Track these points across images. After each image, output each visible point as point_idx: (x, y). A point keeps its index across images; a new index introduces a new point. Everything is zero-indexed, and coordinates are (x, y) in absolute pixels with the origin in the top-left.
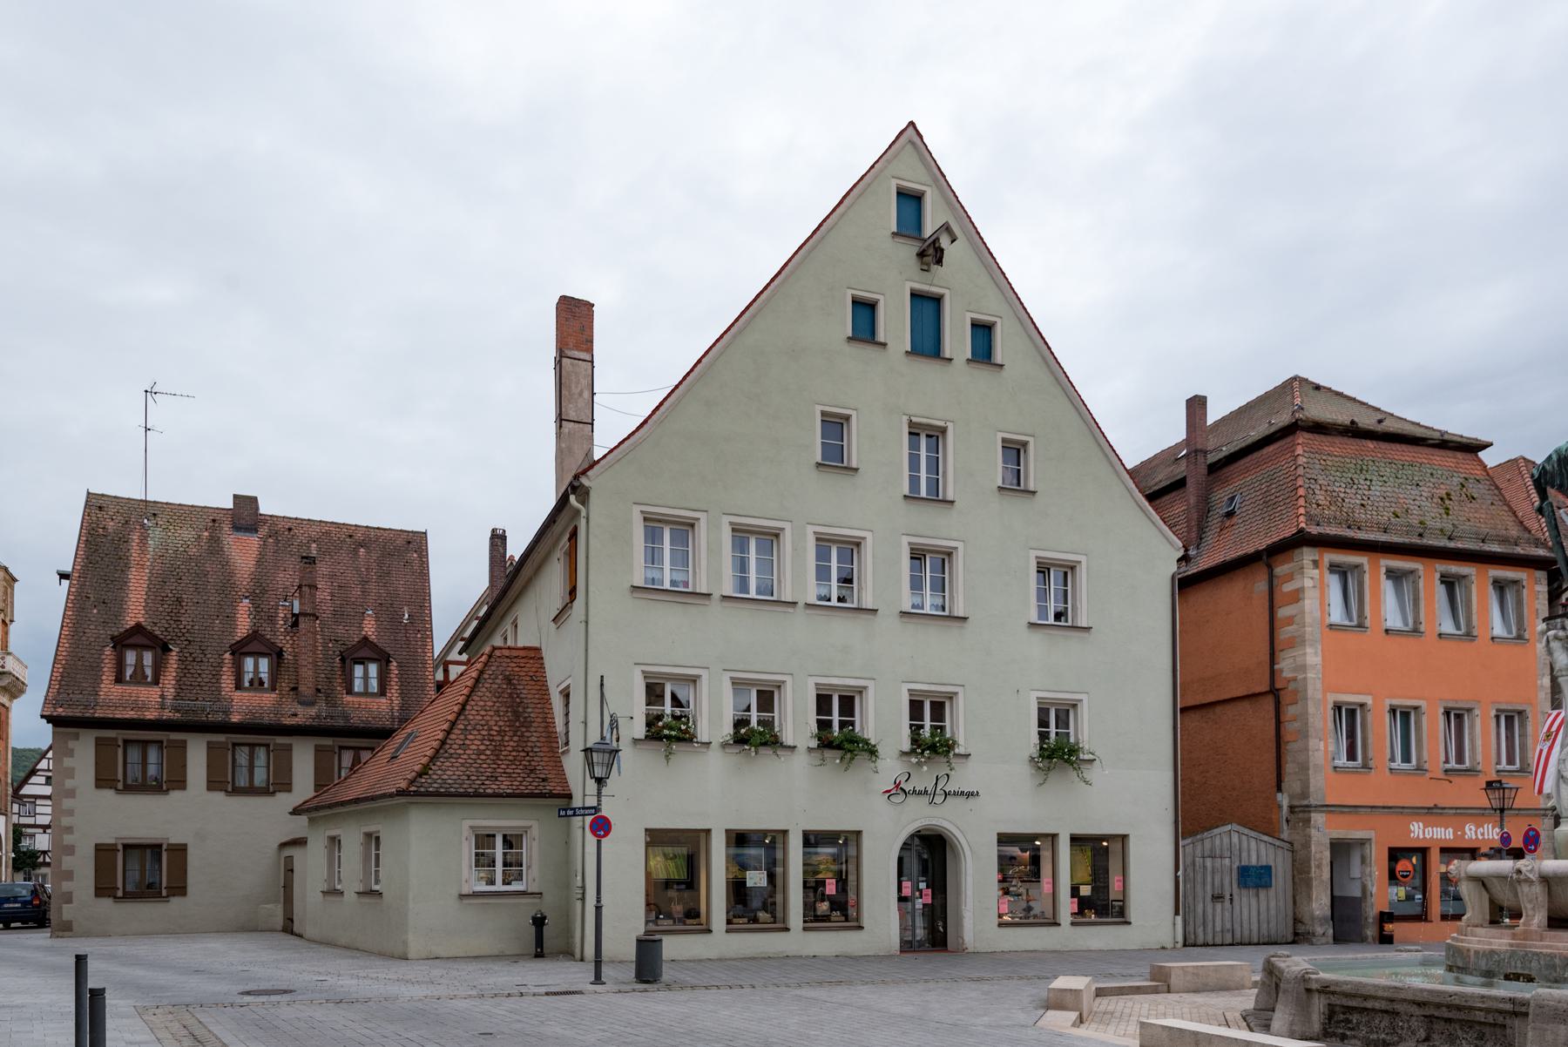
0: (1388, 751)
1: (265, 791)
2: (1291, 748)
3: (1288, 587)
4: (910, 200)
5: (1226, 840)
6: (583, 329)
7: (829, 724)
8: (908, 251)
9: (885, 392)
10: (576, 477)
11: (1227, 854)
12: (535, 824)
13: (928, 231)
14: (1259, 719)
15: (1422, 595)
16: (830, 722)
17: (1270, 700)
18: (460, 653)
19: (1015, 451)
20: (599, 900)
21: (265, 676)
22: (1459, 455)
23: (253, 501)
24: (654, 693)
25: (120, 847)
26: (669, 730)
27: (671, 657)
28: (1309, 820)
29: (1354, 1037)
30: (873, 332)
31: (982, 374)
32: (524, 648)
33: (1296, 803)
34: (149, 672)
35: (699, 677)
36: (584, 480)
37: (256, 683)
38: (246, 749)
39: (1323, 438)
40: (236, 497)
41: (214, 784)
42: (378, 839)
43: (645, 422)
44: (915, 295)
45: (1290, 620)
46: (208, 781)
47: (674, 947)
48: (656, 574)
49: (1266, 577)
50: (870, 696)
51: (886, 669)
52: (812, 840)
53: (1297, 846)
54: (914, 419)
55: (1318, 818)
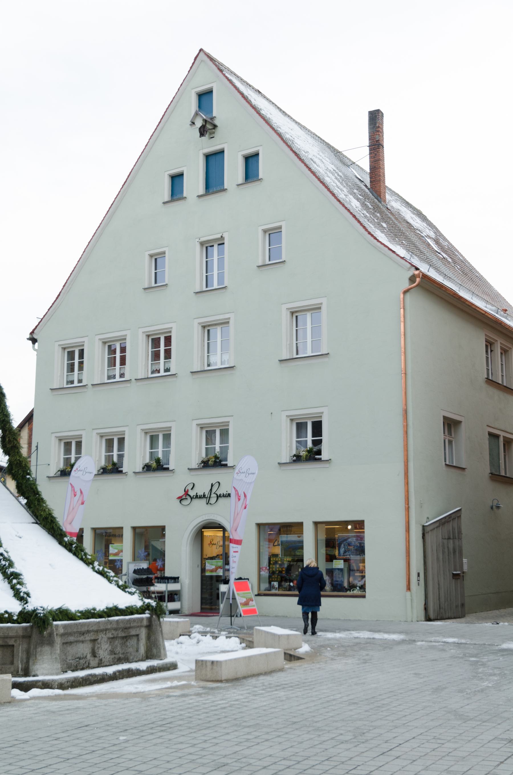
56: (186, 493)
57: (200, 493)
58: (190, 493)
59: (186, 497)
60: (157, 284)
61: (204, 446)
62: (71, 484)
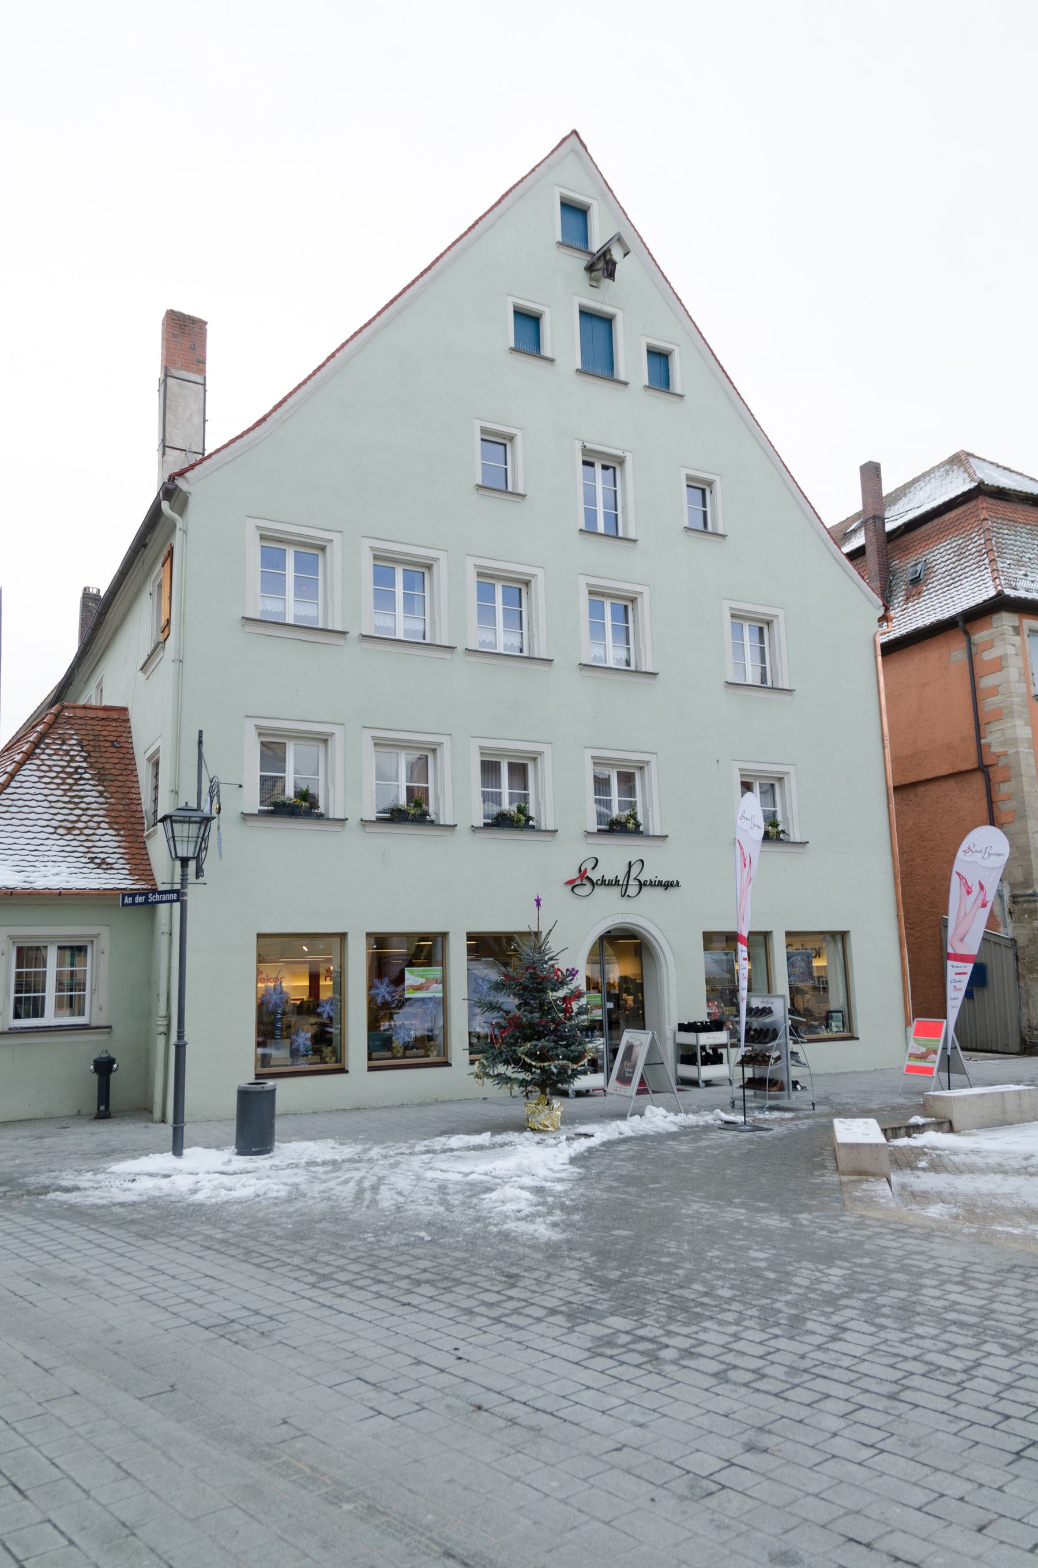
3: (988, 656)
4: (575, 212)
6: (193, 348)
8: (577, 263)
9: (555, 407)
10: (172, 478)
12: (104, 932)
16: (510, 788)
17: (978, 780)
19: (701, 489)
20: (181, 1035)
24: (272, 752)
31: (658, 401)
33: (1017, 892)
36: (180, 482)
39: (1005, 504)
45: (994, 691)
47: (290, 1093)
49: (964, 644)
50: (547, 764)
52: (485, 946)
54: (589, 446)
56: (582, 873)
58: (589, 874)
59: (582, 880)
60: (498, 486)
61: (14, 970)
62: (958, 874)
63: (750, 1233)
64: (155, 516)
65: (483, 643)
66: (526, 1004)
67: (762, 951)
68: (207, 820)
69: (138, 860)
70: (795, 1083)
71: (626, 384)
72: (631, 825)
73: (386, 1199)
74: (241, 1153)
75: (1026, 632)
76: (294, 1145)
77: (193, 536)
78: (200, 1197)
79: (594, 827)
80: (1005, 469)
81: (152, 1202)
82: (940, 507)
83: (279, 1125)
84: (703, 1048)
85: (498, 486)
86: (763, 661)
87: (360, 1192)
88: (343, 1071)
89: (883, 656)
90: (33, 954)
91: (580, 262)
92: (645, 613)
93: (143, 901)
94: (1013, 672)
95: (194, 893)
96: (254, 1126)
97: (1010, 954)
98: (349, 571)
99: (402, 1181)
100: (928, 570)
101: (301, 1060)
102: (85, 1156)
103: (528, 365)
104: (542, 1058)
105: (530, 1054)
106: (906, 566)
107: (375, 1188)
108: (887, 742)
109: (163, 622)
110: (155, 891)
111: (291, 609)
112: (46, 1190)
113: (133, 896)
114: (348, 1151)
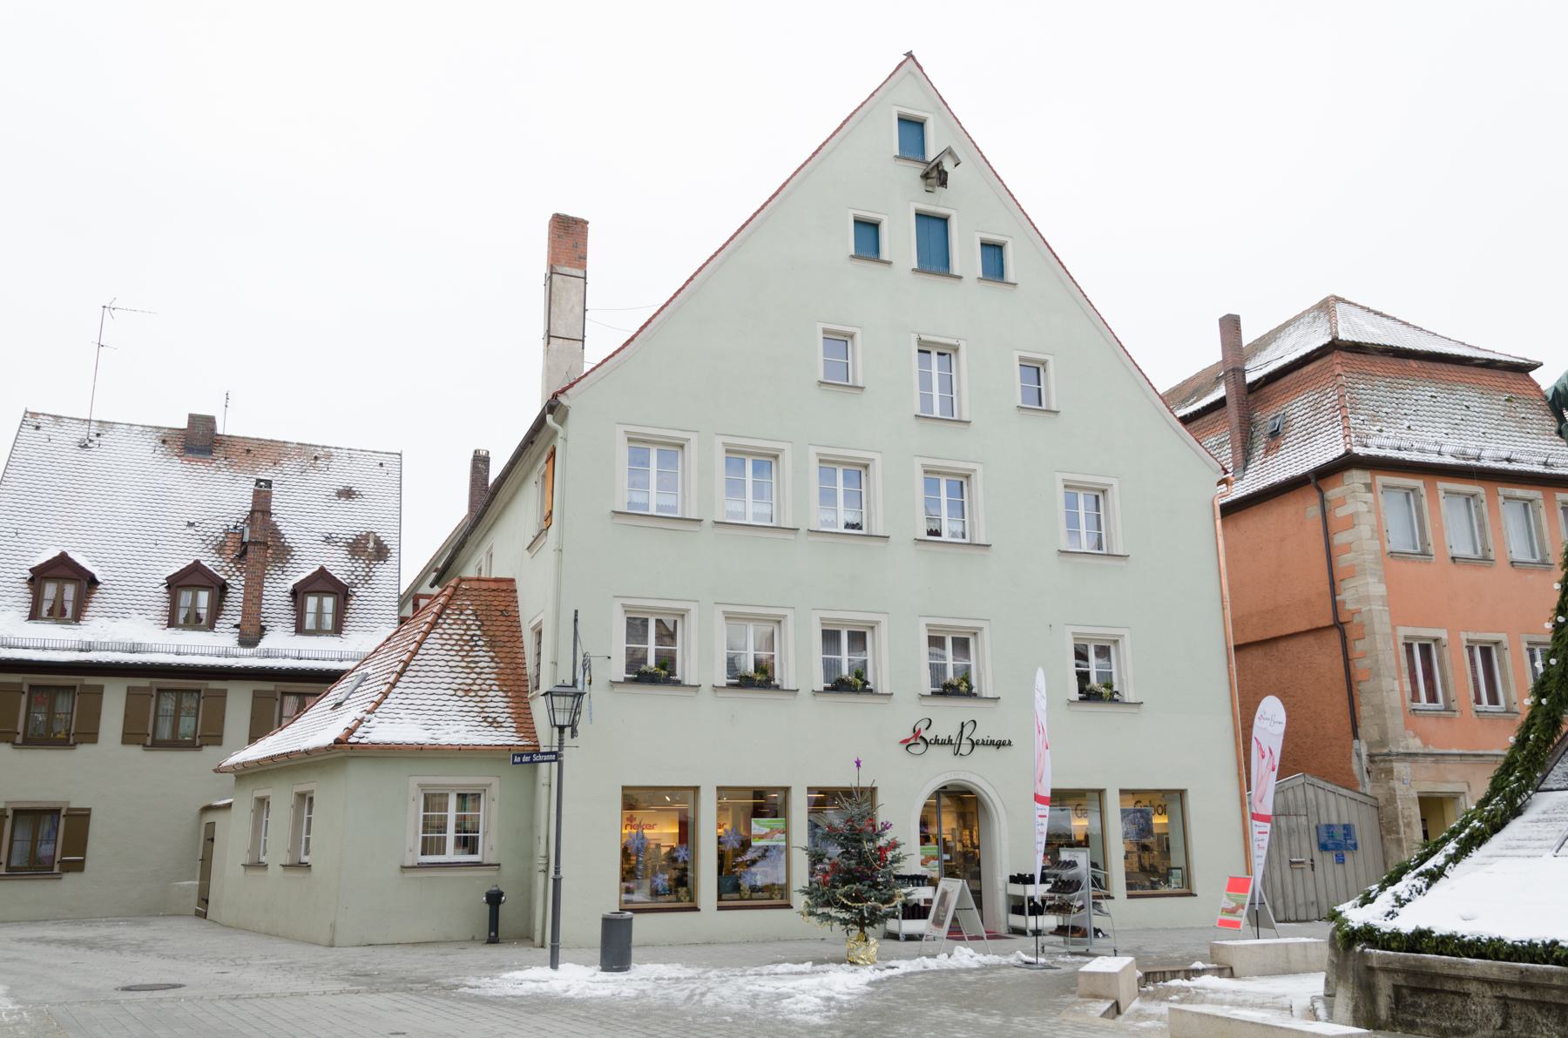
0: (1472, 693)
1: (192, 745)
2: (1364, 688)
3: (1341, 512)
4: (912, 127)
5: (1300, 794)
6: (575, 246)
7: (838, 665)
8: (914, 171)
9: (894, 305)
10: (555, 396)
11: (1303, 811)
12: (495, 782)
13: (931, 155)
14: (1326, 655)
15: (1487, 520)
16: (839, 662)
17: (1336, 634)
18: (432, 586)
19: (1034, 370)
20: (557, 871)
21: (203, 612)
22: (1509, 375)
23: (210, 420)
25: (10, 813)
26: (654, 674)
27: (656, 591)
28: (1391, 771)
29: (1425, 1025)
30: (877, 251)
31: (993, 290)
32: (496, 580)
33: (1374, 751)
34: (69, 607)
35: (688, 610)
37: (193, 618)
38: (173, 697)
40: (192, 417)
41: (131, 736)
42: (311, 799)
43: (632, 339)
44: (921, 216)
45: (1347, 548)
46: (124, 734)
47: (643, 925)
48: (638, 498)
49: (1318, 501)
51: (901, 607)
52: (823, 798)
53: (1382, 802)
54: (924, 338)
55: (1400, 768)
56: (916, 733)
57: (943, 736)
58: (923, 734)
59: (916, 740)
60: (839, 380)
61: (422, 814)
63: (957, 1023)
64: (540, 423)
65: (825, 523)
66: (848, 852)
67: (1178, 806)
68: (581, 694)
69: (524, 721)
70: (1097, 931)
71: (960, 278)
72: (963, 688)
73: (709, 1000)
74: (604, 970)
75: (1379, 488)
76: (649, 967)
77: (572, 440)
78: (571, 994)
79: (928, 690)
80: (1376, 313)
81: (535, 996)
82: (1297, 361)
83: (635, 953)
84: (1031, 899)
85: (839, 380)
86: (1099, 528)
87: (690, 997)
88: (696, 909)
89: (1223, 516)
90: (437, 800)
91: (919, 169)
92: (978, 489)
93: (527, 757)
94: (1364, 530)
95: (567, 755)
96: (615, 949)
97: (933, 830)
98: (704, 461)
99: (725, 991)
100: (1287, 423)
101: (661, 898)
102: (482, 968)
103: (868, 269)
104: (858, 899)
105: (847, 896)
106: (1266, 418)
107: (703, 994)
108: (1228, 605)
109: (546, 512)
110: (538, 753)
111: (654, 501)
112: (457, 987)
113: (521, 756)
114: (690, 972)
